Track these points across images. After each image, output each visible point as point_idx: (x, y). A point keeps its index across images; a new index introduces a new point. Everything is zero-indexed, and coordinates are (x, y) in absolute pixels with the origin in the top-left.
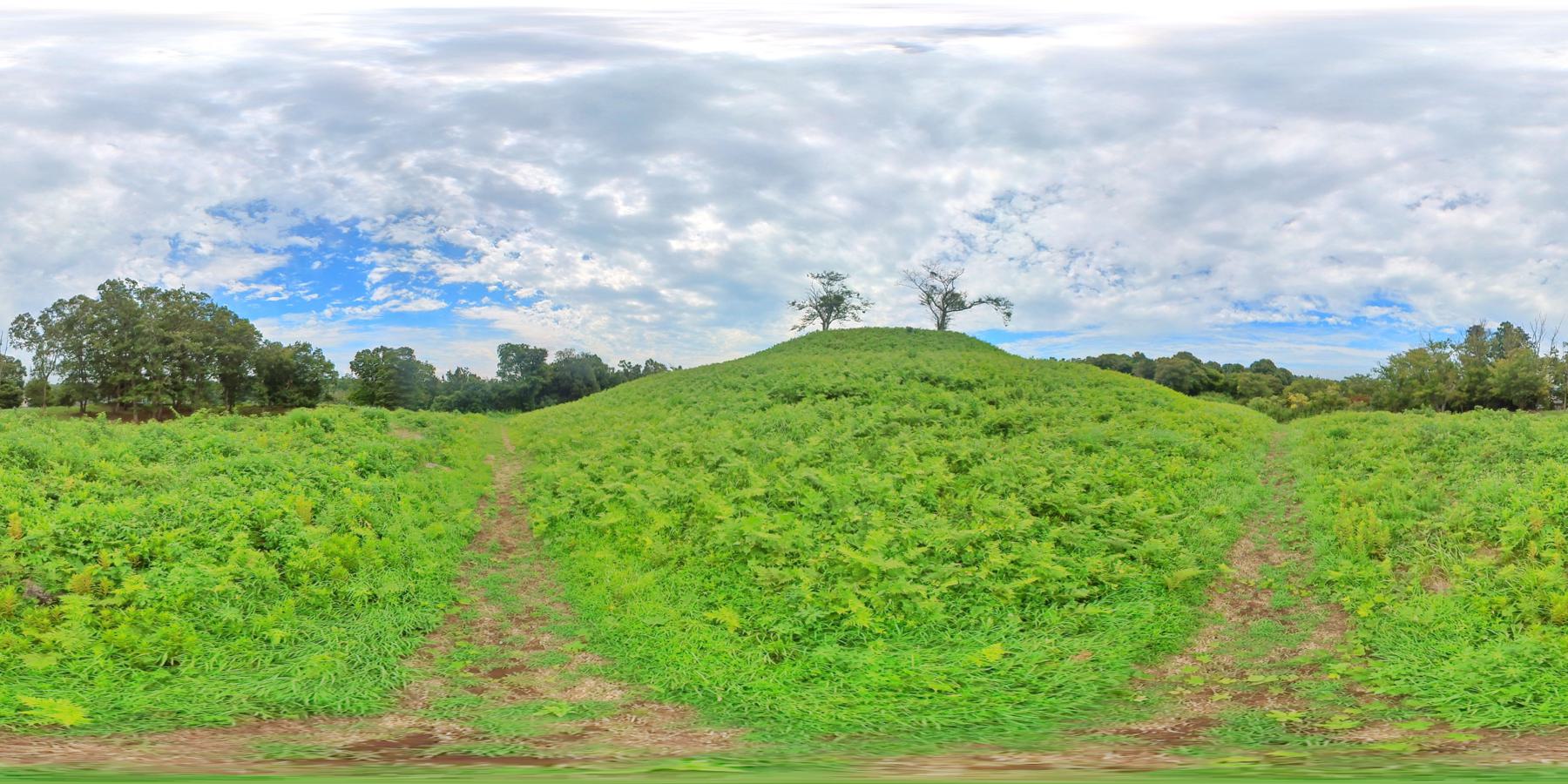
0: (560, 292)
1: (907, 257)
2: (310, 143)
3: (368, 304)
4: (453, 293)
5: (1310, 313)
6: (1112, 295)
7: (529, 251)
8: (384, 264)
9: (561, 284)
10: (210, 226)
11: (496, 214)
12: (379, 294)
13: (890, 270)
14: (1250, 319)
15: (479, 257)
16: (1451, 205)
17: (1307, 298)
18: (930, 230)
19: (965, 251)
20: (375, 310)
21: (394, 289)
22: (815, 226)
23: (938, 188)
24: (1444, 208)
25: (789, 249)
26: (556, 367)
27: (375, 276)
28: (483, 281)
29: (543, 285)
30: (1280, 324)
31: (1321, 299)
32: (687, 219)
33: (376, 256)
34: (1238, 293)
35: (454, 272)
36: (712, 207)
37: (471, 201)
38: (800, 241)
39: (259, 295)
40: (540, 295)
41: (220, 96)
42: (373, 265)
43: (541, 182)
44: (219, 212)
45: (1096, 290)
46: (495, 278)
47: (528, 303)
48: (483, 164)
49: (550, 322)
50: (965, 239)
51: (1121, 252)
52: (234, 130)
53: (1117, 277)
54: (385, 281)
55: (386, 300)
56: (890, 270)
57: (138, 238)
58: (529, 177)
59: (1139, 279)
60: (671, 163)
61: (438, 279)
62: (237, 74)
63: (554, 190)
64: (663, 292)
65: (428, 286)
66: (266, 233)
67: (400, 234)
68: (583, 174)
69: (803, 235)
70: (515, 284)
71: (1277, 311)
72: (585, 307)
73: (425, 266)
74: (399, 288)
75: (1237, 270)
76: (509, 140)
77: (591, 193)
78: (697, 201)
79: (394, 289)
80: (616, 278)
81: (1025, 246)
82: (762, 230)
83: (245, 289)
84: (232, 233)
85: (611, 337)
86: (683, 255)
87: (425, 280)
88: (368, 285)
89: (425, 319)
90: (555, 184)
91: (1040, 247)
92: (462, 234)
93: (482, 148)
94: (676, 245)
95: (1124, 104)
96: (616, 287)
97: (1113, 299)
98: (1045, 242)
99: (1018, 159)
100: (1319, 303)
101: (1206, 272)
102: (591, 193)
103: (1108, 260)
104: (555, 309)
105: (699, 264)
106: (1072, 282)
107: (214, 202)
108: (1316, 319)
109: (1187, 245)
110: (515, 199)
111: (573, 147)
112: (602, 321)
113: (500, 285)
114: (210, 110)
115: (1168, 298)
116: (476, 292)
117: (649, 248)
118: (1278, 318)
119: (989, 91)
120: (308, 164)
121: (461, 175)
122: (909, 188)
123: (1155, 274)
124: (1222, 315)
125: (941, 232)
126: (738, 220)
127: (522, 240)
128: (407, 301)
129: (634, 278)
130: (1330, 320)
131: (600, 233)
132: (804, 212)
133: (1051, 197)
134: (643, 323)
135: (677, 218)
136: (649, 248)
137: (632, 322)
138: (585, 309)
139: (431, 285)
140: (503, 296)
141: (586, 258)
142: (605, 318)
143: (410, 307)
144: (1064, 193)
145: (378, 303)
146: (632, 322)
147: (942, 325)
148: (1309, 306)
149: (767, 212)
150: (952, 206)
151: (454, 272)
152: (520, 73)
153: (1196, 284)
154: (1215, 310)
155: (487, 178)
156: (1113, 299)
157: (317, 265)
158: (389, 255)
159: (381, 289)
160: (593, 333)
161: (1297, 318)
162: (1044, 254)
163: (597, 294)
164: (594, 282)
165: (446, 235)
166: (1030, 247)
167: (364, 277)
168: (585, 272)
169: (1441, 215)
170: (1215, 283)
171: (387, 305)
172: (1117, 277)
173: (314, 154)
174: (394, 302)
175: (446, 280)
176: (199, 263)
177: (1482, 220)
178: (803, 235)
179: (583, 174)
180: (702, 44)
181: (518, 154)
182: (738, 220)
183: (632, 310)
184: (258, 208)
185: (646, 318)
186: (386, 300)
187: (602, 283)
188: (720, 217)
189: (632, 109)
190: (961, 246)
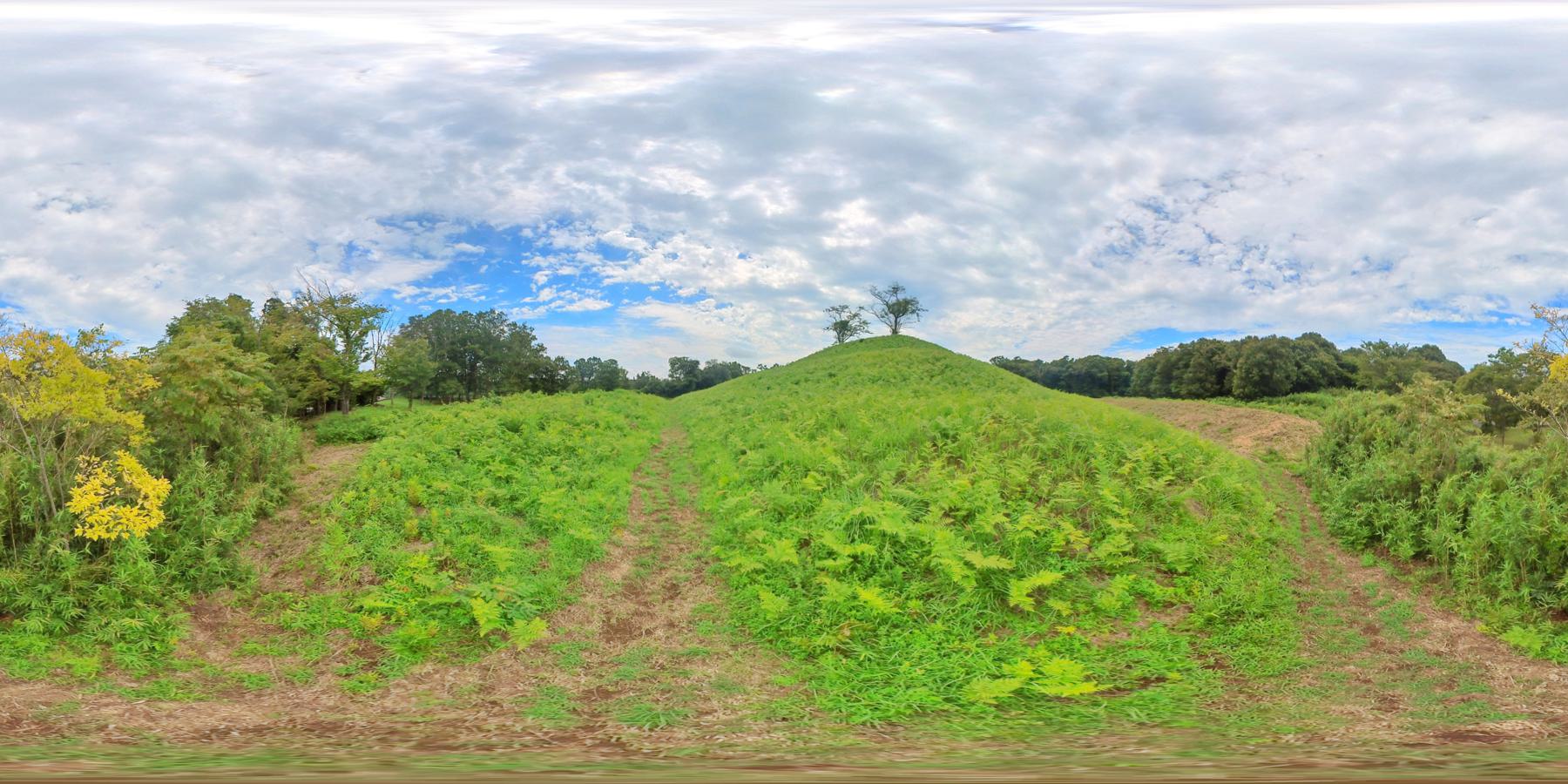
0: (720, 290)
1: (1071, 250)
2: (472, 157)
3: (535, 306)
4: (616, 293)
5: (1491, 313)
6: (1287, 292)
7: (687, 251)
8: (548, 268)
9: (720, 283)
10: (380, 233)
11: (649, 217)
12: (546, 294)
13: (1056, 264)
14: (1429, 319)
15: (638, 258)
16: (76, 208)
17: (1489, 298)
18: (1093, 220)
19: (1134, 244)
20: (542, 309)
21: (558, 290)
22: (975, 218)
23: (1104, 175)
24: (69, 211)
25: (947, 242)
26: (707, 370)
27: (541, 278)
28: (645, 282)
29: (704, 284)
30: (1458, 325)
31: (1503, 298)
32: (835, 215)
33: (538, 260)
34: (1419, 291)
35: (615, 273)
36: (862, 202)
37: (624, 206)
38: (963, 236)
39: (431, 297)
40: (702, 295)
41: (396, 116)
42: (538, 268)
43: (40, 194)
44: (387, 222)
45: (1271, 286)
46: (655, 278)
47: (691, 300)
48: (626, 172)
49: (714, 320)
50: (1134, 229)
51: (1299, 244)
52: (403, 147)
53: (1292, 273)
54: (549, 284)
55: (551, 301)
56: (1056, 264)
57: (314, 246)
58: (668, 179)
59: (1316, 275)
60: (812, 160)
61: (600, 281)
62: (407, 94)
63: (699, 193)
64: (823, 290)
65: (591, 287)
66: (433, 240)
67: (561, 239)
68: (726, 176)
69: (961, 229)
70: (676, 284)
71: (1456, 311)
72: (747, 305)
73: (587, 269)
74: (563, 290)
75: (1420, 265)
76: (649, 145)
77: (736, 193)
78: (849, 195)
79: (558, 290)
80: (775, 278)
81: (1196, 239)
82: (915, 224)
83: (417, 291)
84: (399, 238)
85: (776, 334)
86: (838, 252)
87: (587, 280)
88: (534, 287)
89: (587, 318)
90: (701, 188)
91: (1211, 239)
92: (618, 235)
93: (624, 158)
94: (829, 242)
95: (1344, 84)
96: (775, 286)
97: (1289, 296)
98: (1216, 233)
99: (1188, 140)
100: (1502, 303)
101: (1387, 267)
102: (736, 193)
103: (1284, 254)
104: (718, 307)
105: (856, 261)
106: (1246, 277)
107: (386, 213)
108: (1495, 319)
109: (1369, 238)
110: (666, 202)
111: (711, 151)
112: (766, 318)
113: (661, 284)
114: (384, 128)
115: (1345, 296)
116: (639, 292)
117: (805, 246)
118: (1456, 318)
119: (1152, 69)
120: (471, 178)
121: (611, 183)
122: (1070, 174)
123: (1334, 270)
124: (1400, 314)
125: (1108, 223)
126: (891, 215)
127: (679, 241)
128: (571, 302)
129: (792, 276)
130: (1511, 321)
131: (753, 233)
132: (961, 204)
133: (1226, 183)
134: (809, 321)
135: (827, 215)
136: (805, 246)
137: (797, 320)
138: (748, 307)
139: (594, 286)
140: (665, 293)
141: (742, 256)
142: (769, 315)
143: (576, 308)
144: (1238, 181)
145: (544, 303)
146: (797, 320)
147: (895, 332)
148: (1490, 306)
149: (919, 205)
150: (1116, 192)
151: (615, 273)
152: (620, 85)
153: (1375, 281)
154: (1393, 309)
155: (633, 182)
156: (1289, 296)
157: (484, 269)
158: (552, 259)
159: (547, 291)
160: (757, 330)
161: (1477, 318)
162: (1216, 247)
163: (756, 291)
164: (753, 281)
165: (605, 238)
166: (1202, 238)
167: (530, 280)
168: (742, 272)
169: (66, 217)
170: (1395, 279)
171: (553, 305)
172: (1292, 273)
173: (476, 167)
174: (559, 302)
175: (607, 282)
176: (370, 266)
177: (105, 224)
178: (961, 229)
179: (726, 176)
180: (467, 42)
181: (660, 158)
182: (891, 215)
183: (793, 307)
184: (427, 220)
185: (809, 316)
186: (551, 301)
187: (761, 281)
188: (871, 211)
189: (755, 112)
190: (1129, 237)
